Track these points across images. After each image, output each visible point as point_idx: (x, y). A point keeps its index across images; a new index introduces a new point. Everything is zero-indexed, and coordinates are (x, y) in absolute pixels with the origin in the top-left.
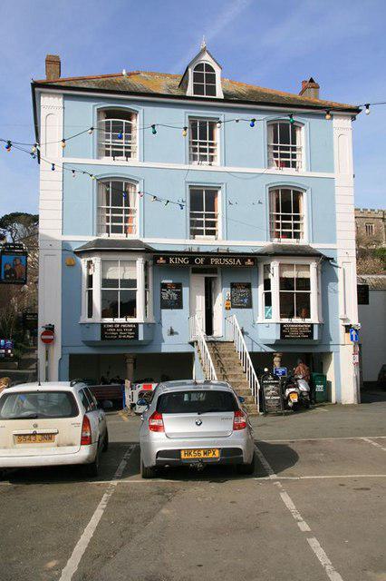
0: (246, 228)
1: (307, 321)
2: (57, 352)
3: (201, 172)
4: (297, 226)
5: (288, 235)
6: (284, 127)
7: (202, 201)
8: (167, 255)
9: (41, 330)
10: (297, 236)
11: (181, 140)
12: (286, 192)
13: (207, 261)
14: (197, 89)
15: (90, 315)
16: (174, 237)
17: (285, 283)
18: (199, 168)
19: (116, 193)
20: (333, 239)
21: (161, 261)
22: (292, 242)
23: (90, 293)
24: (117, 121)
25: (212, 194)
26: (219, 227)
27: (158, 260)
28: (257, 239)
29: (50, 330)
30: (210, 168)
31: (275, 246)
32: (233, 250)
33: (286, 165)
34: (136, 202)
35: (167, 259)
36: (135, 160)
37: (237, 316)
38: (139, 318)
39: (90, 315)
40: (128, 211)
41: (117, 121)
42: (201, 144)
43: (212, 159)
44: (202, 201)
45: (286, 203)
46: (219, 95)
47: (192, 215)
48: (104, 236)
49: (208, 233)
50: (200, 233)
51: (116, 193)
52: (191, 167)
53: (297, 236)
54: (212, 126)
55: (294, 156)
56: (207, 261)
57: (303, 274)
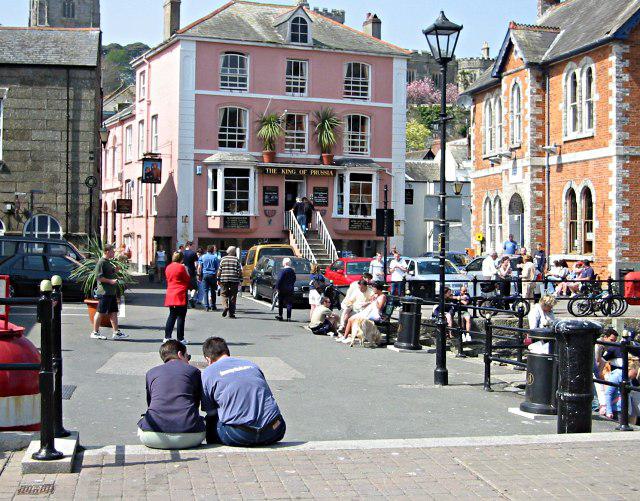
1: (244, 214)
4: (363, 144)
18: (293, 99)
38: (251, 213)
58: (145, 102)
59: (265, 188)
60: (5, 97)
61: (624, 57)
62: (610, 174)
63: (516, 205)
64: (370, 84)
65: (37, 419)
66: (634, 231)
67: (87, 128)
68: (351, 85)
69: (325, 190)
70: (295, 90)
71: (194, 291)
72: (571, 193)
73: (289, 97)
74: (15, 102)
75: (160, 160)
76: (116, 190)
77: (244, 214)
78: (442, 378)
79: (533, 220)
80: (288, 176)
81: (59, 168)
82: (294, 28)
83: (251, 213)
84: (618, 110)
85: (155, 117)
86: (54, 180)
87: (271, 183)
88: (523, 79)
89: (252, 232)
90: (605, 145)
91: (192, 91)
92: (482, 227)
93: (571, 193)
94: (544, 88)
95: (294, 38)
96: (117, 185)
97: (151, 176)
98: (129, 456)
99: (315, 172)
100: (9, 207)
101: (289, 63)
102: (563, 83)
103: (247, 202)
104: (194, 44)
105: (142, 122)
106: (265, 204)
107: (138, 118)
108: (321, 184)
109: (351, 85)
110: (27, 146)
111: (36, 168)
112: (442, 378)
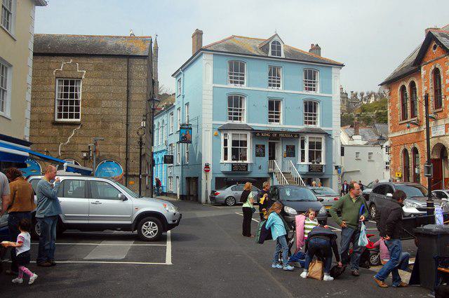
0: (290, 120)
1: (245, 162)
2: (210, 175)
3: (274, 92)
4: (315, 119)
5: (311, 123)
6: (236, 63)
7: (274, 106)
8: (261, 132)
9: (203, 166)
10: (315, 123)
11: (301, 78)
12: (311, 103)
13: (278, 135)
14: (273, 53)
15: (226, 159)
16: (263, 124)
17: (235, 143)
18: (273, 90)
19: (235, 102)
20: (331, 126)
21: (258, 135)
22: (237, 122)
23: (226, 150)
24: (236, 71)
25: (278, 103)
26: (281, 118)
27: (256, 134)
28: (299, 126)
29: (207, 166)
30: (277, 91)
31: (306, 128)
32: (289, 130)
33: (310, 89)
34: (319, 112)
35: (260, 134)
36: (318, 93)
37: (290, 161)
38: (248, 161)
39: (226, 159)
40: (241, 110)
41: (236, 71)
42: (240, 75)
43: (279, 86)
44: (274, 106)
45: (310, 107)
46: (283, 56)
47: (269, 113)
48: (230, 122)
49: (276, 121)
50: (273, 121)
51: (235, 102)
52: (270, 90)
53: (315, 123)
54: (315, 72)
55: (314, 86)
56: (278, 135)
57: (243, 139)
58: (181, 97)
60: (83, 77)
64: (281, 114)
67: (141, 99)
68: (274, 115)
70: (274, 85)
71: (24, 235)
72: (405, 151)
73: (270, 89)
74: (91, 81)
75: (191, 129)
76: (163, 151)
77: (245, 162)
81: (121, 126)
83: (248, 161)
85: (187, 104)
86: (118, 135)
87: (260, 143)
93: (405, 151)
96: (165, 148)
97: (185, 139)
100: (85, 155)
105: (179, 109)
107: (177, 107)
109: (274, 115)
110: (94, 111)
111: (104, 127)
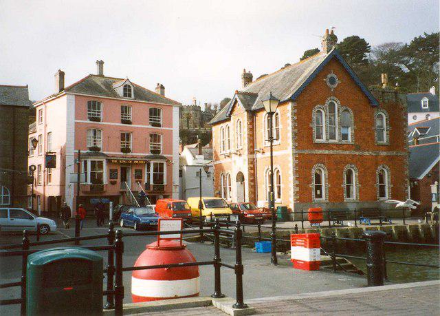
59: (111, 170)
61: (294, 108)
62: (289, 162)
63: (240, 177)
65: (124, 273)
66: (301, 189)
69: (141, 171)
78: (101, 63)
79: (249, 184)
80: (122, 164)
82: (125, 90)
84: (293, 132)
88: (242, 117)
89: (105, 192)
90: (286, 149)
91: (73, 121)
92: (219, 188)
94: (253, 121)
95: (125, 95)
98: (268, 256)
99: (137, 162)
101: (122, 107)
102: (263, 120)
103: (102, 173)
104: (74, 96)
106: (110, 178)
108: (139, 168)
112: (101, 63)
